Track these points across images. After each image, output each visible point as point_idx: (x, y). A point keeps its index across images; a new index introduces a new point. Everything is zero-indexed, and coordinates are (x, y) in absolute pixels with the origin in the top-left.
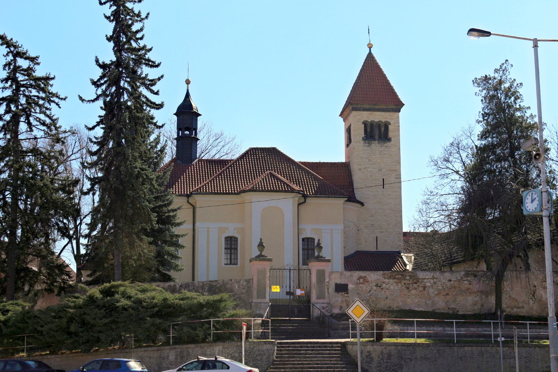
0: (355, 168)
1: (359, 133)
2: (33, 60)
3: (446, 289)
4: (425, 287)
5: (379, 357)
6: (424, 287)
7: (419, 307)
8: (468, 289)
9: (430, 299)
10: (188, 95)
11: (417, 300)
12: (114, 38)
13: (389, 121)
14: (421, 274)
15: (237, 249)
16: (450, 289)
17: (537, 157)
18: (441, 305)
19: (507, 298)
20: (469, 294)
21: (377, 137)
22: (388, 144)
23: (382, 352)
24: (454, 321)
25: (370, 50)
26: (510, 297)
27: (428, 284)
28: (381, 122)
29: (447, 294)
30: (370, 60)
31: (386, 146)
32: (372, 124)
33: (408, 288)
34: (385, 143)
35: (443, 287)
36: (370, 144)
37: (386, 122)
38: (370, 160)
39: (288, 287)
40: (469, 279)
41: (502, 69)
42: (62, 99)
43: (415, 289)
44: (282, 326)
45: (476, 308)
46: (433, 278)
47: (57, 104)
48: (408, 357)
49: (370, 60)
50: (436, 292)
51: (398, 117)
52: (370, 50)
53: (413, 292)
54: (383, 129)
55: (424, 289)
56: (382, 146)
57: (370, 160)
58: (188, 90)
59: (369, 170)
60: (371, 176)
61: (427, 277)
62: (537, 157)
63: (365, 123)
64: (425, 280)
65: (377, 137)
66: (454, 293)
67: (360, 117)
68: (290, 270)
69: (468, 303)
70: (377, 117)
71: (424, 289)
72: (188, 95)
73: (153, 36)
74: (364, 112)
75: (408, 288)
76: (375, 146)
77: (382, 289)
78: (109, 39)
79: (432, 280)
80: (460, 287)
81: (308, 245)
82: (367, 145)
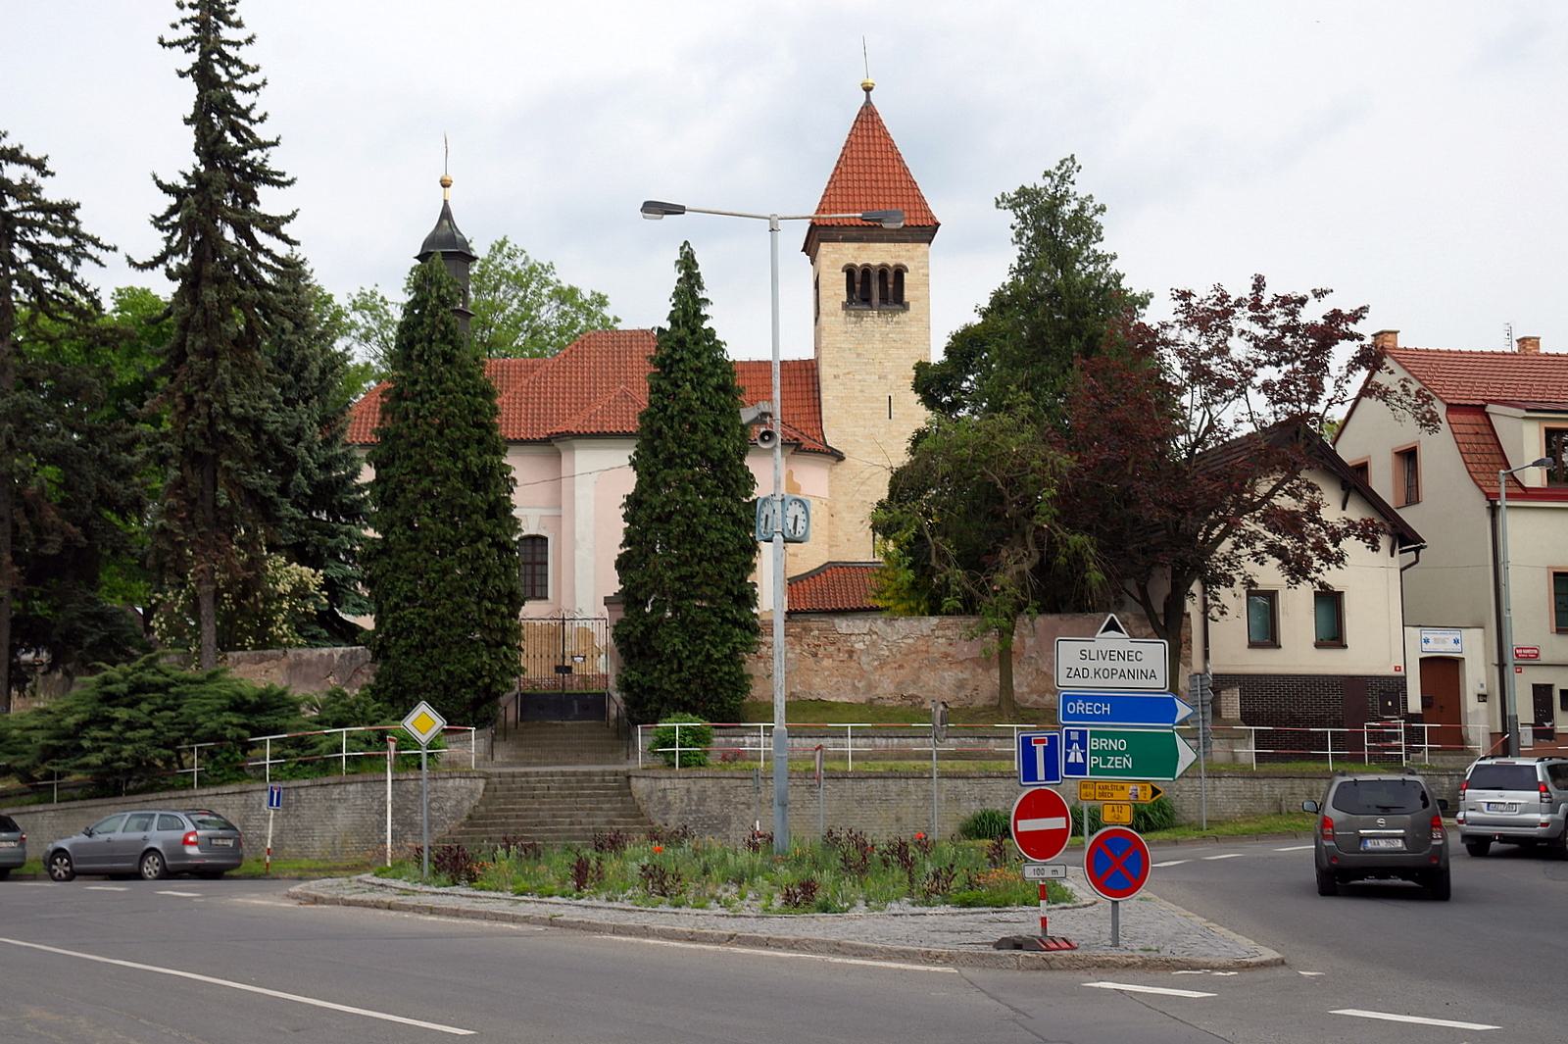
0: (826, 372)
1: (836, 289)
2: (39, 166)
3: (898, 656)
4: (853, 652)
5: (682, 801)
6: (851, 653)
7: (838, 696)
8: (946, 655)
9: (862, 676)
10: (446, 214)
11: (835, 680)
12: (199, 119)
13: (904, 263)
14: (844, 625)
15: (546, 564)
16: (906, 655)
17: (767, 438)
18: (886, 687)
19: (1031, 673)
20: (947, 665)
21: (876, 299)
22: (902, 317)
23: (688, 791)
24: (268, 738)
25: (868, 96)
26: (1037, 670)
27: (860, 646)
28: (887, 266)
29: (901, 667)
30: (868, 119)
31: (897, 323)
32: (866, 270)
33: (815, 655)
34: (894, 312)
35: (890, 650)
36: (859, 317)
37: (882, 265)
38: (858, 355)
39: (559, 657)
40: (949, 633)
41: (1065, 171)
42: (107, 249)
43: (830, 656)
44: (1378, 727)
45: (962, 695)
46: (871, 632)
47: (97, 261)
48: (743, 799)
49: (868, 119)
50: (876, 663)
51: (926, 254)
52: (868, 96)
53: (827, 663)
54: (891, 279)
55: (851, 657)
56: (888, 323)
57: (858, 355)
58: (446, 202)
59: (857, 377)
60: (862, 391)
61: (857, 632)
62: (767, 438)
63: (850, 271)
64: (853, 638)
65: (876, 299)
66: (916, 665)
67: (840, 255)
68: (564, 619)
69: (941, 684)
70: (877, 254)
71: (851, 657)
72: (446, 214)
73: (282, 112)
74: (847, 245)
75: (815, 655)
76: (874, 322)
77: (759, 657)
78: (187, 122)
79: (867, 638)
80: (927, 652)
81: (533, 574)
82: (853, 319)
